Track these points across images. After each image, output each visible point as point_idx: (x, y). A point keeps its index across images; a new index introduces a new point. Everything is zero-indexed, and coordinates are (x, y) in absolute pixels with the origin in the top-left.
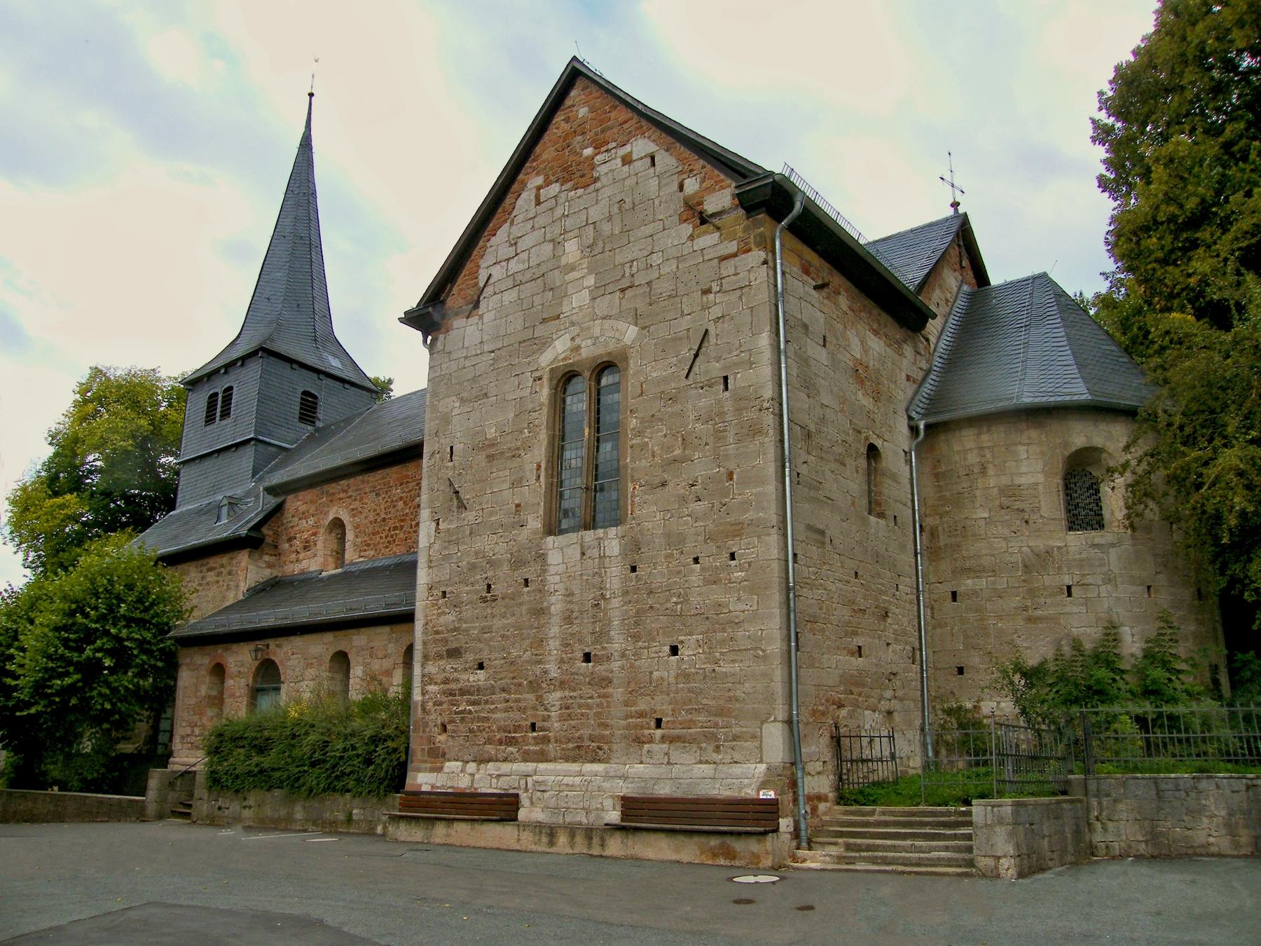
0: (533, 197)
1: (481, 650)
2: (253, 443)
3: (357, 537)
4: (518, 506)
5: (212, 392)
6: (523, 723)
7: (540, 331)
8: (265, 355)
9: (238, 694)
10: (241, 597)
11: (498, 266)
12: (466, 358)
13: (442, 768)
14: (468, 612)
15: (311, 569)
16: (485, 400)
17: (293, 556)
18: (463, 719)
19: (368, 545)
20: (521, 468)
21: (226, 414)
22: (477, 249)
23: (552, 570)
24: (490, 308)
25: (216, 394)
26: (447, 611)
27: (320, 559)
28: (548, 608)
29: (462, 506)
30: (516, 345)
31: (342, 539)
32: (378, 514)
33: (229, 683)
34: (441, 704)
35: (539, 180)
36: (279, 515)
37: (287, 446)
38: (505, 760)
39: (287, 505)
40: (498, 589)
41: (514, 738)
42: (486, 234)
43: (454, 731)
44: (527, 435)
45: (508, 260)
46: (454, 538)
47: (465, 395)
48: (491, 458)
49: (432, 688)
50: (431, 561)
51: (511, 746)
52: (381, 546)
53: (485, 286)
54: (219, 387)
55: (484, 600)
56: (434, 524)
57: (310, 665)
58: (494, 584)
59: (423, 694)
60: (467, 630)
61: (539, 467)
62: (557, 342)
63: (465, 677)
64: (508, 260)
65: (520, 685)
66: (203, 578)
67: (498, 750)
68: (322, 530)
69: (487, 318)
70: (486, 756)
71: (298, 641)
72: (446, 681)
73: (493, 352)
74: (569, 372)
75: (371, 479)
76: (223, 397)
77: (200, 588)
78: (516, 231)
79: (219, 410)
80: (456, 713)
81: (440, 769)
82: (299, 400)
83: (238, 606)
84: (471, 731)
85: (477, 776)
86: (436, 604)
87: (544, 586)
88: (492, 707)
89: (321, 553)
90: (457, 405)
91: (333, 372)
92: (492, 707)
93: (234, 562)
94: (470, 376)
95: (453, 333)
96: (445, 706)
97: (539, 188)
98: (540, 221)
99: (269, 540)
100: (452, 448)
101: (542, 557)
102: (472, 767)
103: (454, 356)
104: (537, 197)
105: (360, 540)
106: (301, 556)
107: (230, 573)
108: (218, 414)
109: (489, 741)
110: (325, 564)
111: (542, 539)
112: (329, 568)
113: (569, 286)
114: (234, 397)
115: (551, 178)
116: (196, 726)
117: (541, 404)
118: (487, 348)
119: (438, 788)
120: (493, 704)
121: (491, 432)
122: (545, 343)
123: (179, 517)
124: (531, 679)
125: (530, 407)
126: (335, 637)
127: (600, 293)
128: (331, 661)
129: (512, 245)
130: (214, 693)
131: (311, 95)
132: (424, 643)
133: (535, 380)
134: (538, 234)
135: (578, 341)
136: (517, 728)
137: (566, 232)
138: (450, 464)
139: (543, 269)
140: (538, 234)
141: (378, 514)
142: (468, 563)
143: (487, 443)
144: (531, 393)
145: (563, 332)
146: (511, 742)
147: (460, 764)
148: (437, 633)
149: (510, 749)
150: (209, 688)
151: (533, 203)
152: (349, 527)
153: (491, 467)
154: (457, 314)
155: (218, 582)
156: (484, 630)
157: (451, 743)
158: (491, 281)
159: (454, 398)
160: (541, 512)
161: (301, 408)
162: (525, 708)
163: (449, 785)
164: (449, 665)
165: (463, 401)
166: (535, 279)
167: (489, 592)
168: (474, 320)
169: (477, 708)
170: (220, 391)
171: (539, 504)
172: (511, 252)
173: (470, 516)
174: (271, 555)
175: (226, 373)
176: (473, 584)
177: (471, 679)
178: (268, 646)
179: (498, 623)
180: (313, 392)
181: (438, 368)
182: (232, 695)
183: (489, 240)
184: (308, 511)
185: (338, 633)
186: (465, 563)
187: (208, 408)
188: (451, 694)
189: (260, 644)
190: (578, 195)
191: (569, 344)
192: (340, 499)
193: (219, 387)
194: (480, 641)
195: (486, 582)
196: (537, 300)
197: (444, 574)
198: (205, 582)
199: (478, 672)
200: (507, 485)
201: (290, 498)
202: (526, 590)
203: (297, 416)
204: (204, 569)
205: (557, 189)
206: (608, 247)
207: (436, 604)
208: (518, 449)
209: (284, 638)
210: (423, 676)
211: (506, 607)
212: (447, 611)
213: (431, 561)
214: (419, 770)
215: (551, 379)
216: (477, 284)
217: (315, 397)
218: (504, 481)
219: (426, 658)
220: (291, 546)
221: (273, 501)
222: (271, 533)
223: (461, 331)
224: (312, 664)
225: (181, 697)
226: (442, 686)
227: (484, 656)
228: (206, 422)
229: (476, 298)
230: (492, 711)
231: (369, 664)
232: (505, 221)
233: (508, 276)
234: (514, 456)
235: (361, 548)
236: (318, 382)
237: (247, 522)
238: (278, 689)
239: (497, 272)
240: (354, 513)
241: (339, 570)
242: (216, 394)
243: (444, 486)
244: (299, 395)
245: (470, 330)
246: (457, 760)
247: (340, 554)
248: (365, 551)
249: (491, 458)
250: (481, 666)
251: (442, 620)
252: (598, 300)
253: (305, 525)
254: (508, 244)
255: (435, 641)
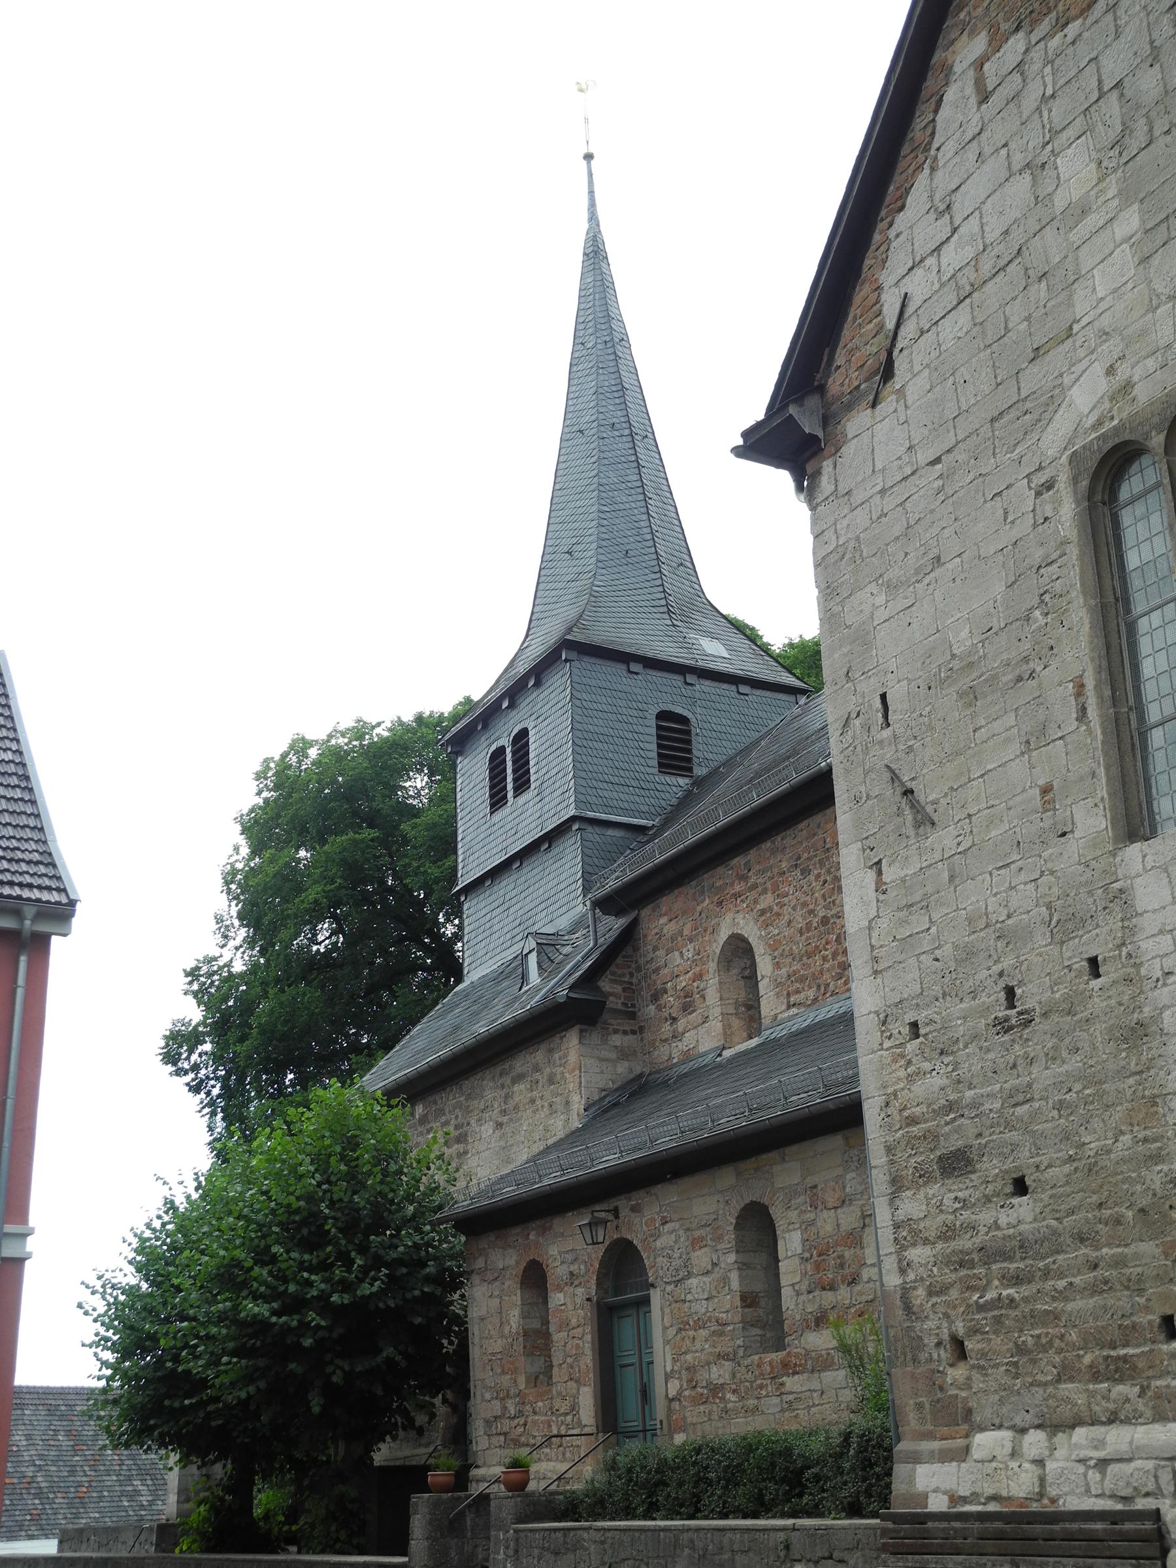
0: (970, 90)
1: (1014, 1147)
2: (575, 827)
3: (777, 966)
4: (1046, 790)
5: (493, 748)
6: (1143, 1319)
7: (1034, 378)
8: (573, 655)
9: (574, 1322)
10: (576, 1124)
11: (919, 272)
12: (883, 492)
13: (967, 1449)
14: (972, 1061)
15: (702, 1049)
16: (938, 572)
17: (667, 1027)
18: (998, 1320)
19: (802, 980)
20: (1039, 700)
21: (522, 784)
22: (870, 254)
23: (1149, 923)
24: (917, 368)
25: (501, 751)
26: (927, 1066)
27: (716, 1026)
28: (1156, 1019)
29: (925, 821)
30: (986, 431)
31: (751, 978)
32: (811, 912)
33: (557, 1299)
34: (943, 1290)
35: (978, 45)
36: (629, 950)
37: (643, 822)
38: (1113, 1419)
39: (644, 924)
40: (1031, 996)
41: (1125, 1359)
42: (883, 213)
43: (983, 1354)
44: (1042, 621)
45: (938, 249)
46: (917, 896)
47: (894, 574)
48: (971, 696)
49: (918, 1254)
50: (876, 960)
51: (1121, 1381)
52: (826, 976)
53: (898, 326)
54: (502, 736)
55: (1003, 1026)
56: (871, 875)
57: (697, 1243)
58: (1021, 983)
59: (903, 1271)
60: (975, 1104)
61: (1080, 688)
62: (1075, 392)
63: (986, 1217)
64: (938, 249)
65: (1118, 1221)
66: (507, 1097)
67: (1092, 1394)
68: (712, 966)
69: (912, 394)
70: (1065, 1412)
71: (669, 1195)
72: (948, 1233)
73: (937, 461)
74: (1116, 448)
75: (788, 841)
76: (514, 753)
77: (505, 1119)
78: (944, 180)
79: (510, 778)
80: (981, 1308)
81: (964, 1453)
82: (654, 731)
83: (573, 1137)
84: (1021, 1349)
85: (1050, 1466)
86: (902, 1056)
87: (1137, 966)
88: (1061, 1284)
89: (716, 1012)
90: (881, 599)
91: (712, 666)
92: (1061, 1284)
93: (557, 1056)
94: (897, 530)
95: (848, 450)
96: (954, 1294)
97: (979, 64)
98: (997, 133)
99: (614, 1003)
100: (883, 697)
101: (1121, 898)
102: (1035, 1441)
103: (858, 498)
104: (980, 83)
105: (784, 972)
106: (681, 1025)
107: (551, 1081)
108: (510, 786)
109: (1066, 1373)
110: (727, 1033)
111: (1113, 854)
112: (736, 1039)
113: (1083, 252)
114: (532, 748)
115: (1004, 26)
116: (508, 1396)
117: (1065, 542)
118: (923, 457)
119: (964, 1500)
120: (1061, 1275)
121: (963, 639)
122: (1053, 400)
123: (466, 994)
124: (1144, 1202)
125: (1038, 555)
126: (738, 1174)
127: (1159, 242)
128: (738, 1227)
129: (942, 213)
130: (536, 1324)
131: (589, 157)
132: (889, 1149)
133: (1038, 494)
134: (995, 166)
135: (1123, 372)
136: (1129, 1334)
137: (1055, 133)
138: (887, 733)
139: (1017, 237)
140: (995, 166)
141: (811, 912)
142: (956, 947)
143: (956, 664)
144: (1035, 525)
145: (1085, 363)
146: (1121, 1370)
147: (1006, 1435)
148: (912, 1121)
149: (1121, 1389)
150: (525, 1316)
151: (973, 101)
152: (759, 949)
153: (974, 716)
154: (849, 407)
155: (533, 1101)
156: (1020, 1096)
157: (978, 1384)
158: (910, 310)
159: (873, 588)
160: (1103, 792)
161: (659, 746)
162: (1140, 1278)
163: (989, 1491)
164: (946, 1192)
165: (891, 588)
166: (1003, 269)
167: (1011, 1006)
168: (888, 404)
169: (1026, 1290)
170: (505, 741)
171: (1093, 775)
172: (941, 229)
173: (944, 839)
174: (625, 1033)
175: (512, 706)
176: (974, 994)
177: (1003, 1221)
178: (616, 1212)
179: (1042, 1076)
180: (678, 710)
181: (830, 535)
182: (565, 1325)
183: (891, 225)
184: (681, 933)
185: (742, 1165)
186: (948, 948)
187: (491, 779)
188: (961, 1264)
189: (601, 1211)
190: (1069, 39)
191: (1103, 385)
192: (736, 896)
193: (502, 736)
194: (1009, 1126)
195: (1002, 984)
196: (1016, 312)
197: (908, 982)
198: (511, 1104)
199: (1016, 1201)
200: (1016, 748)
201: (645, 912)
202: (1096, 984)
203: (655, 763)
204: (507, 1080)
205: (1021, 47)
206: (1160, 127)
207: (902, 1056)
208: (1026, 660)
209: (642, 1193)
210: (897, 1226)
211: (1058, 1034)
212: (927, 1066)
213: (876, 960)
214: (916, 1458)
215: (1075, 480)
216: (881, 326)
217: (684, 720)
218: (1008, 740)
219: (897, 1184)
220: (659, 1008)
221: (614, 925)
222: (618, 989)
223: (866, 437)
224: (702, 1239)
225: (476, 1340)
226: (940, 1246)
227: (1024, 1160)
228: (492, 805)
229: (883, 356)
230: (1062, 1296)
231: (812, 1223)
232: (920, 168)
233: (942, 285)
234: (1020, 679)
235: (788, 990)
236: (687, 691)
237: (569, 974)
238: (646, 1301)
239: (919, 286)
240: (766, 917)
241: (754, 1042)
242: (501, 751)
243: (880, 786)
244: (653, 722)
245: (881, 430)
246: (1000, 1427)
247: (750, 1010)
248: (798, 992)
249: (971, 696)
250: (1020, 1187)
251: (920, 1089)
252: (1156, 261)
253: (678, 961)
254: (932, 216)
255: (910, 1141)
